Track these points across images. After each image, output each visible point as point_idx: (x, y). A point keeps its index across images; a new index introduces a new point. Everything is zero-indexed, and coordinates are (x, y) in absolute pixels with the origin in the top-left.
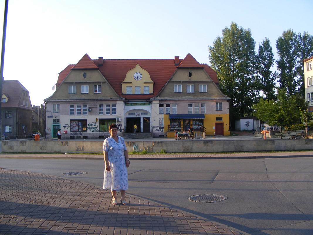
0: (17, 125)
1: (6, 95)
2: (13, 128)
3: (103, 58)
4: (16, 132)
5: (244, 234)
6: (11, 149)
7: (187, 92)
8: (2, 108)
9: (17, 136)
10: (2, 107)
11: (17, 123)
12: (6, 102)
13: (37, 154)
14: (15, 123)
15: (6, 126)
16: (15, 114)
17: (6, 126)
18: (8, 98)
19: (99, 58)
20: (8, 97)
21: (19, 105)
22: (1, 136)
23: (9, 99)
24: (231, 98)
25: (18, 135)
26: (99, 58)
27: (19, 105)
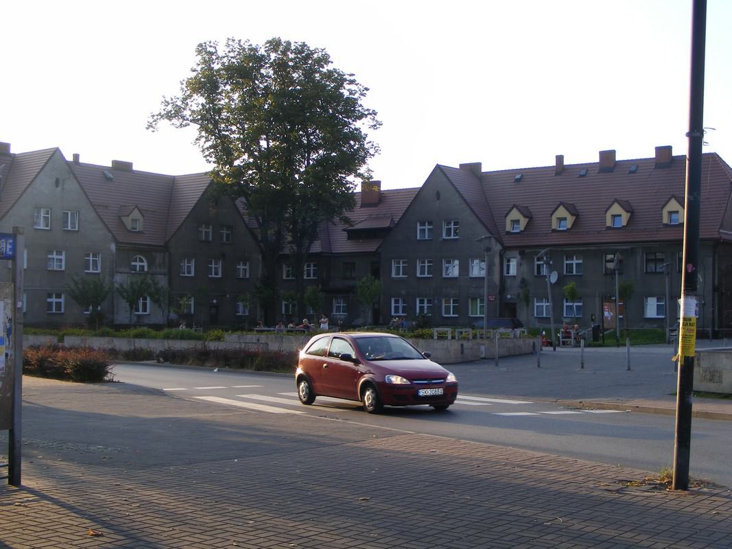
0: (716, 294)
1: (622, 206)
2: (704, 304)
3: (478, 165)
4: (713, 319)
5: (148, 544)
6: (711, 380)
7: (50, 269)
8: (702, 240)
9: (716, 329)
10: (700, 237)
11: (715, 289)
12: (624, 226)
13: (721, 398)
14: (711, 288)
15: (649, 299)
16: (710, 260)
17: (647, 298)
18: (629, 214)
19: (659, 150)
20: (627, 211)
21: (721, 231)
22: (667, 330)
23: (529, 221)
24: (454, 258)
25: (718, 328)
26: (659, 150)
27: (721, 231)
